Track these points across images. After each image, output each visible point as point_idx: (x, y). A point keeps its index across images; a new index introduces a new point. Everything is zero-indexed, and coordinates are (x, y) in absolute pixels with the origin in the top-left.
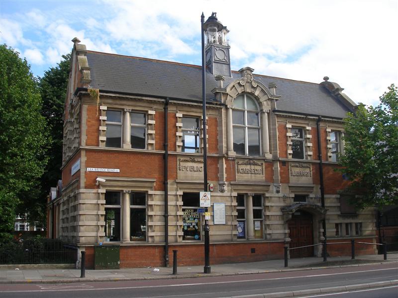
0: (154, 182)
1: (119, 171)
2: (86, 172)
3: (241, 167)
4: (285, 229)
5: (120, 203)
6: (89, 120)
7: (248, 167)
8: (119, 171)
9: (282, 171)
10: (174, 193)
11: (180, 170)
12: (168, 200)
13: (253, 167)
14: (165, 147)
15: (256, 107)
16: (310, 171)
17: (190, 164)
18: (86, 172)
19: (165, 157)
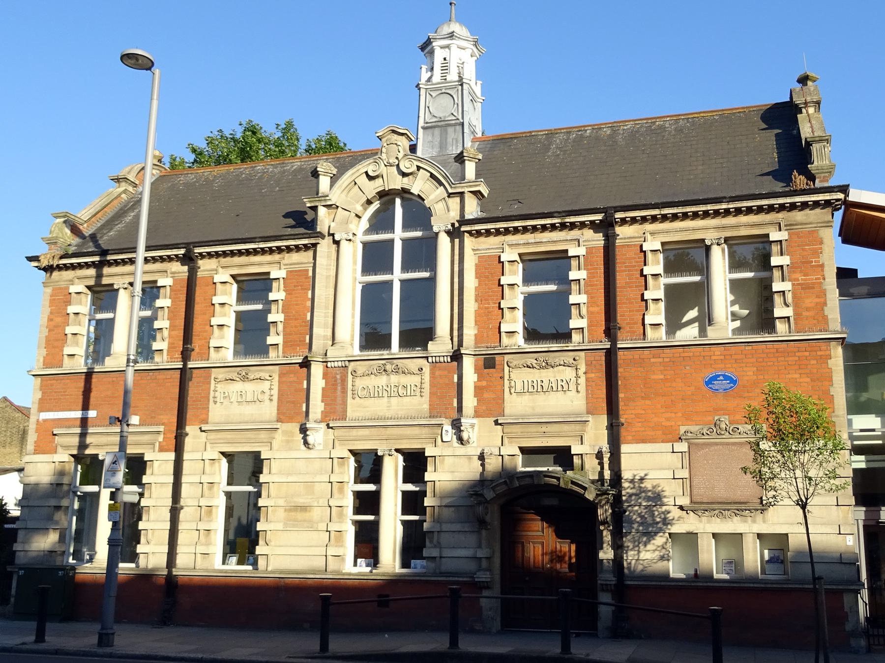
0: (158, 432)
1: (458, 240)
2: (38, 421)
3: (360, 383)
4: (480, 546)
5: (13, 529)
6: (52, 317)
7: (382, 380)
8: (458, 240)
9: (484, 383)
10: (198, 456)
11: (215, 402)
12: (184, 472)
13: (394, 379)
14: (186, 355)
15: (64, 281)
16: (577, 377)
17: (239, 386)
18: (38, 421)
19: (185, 374)
